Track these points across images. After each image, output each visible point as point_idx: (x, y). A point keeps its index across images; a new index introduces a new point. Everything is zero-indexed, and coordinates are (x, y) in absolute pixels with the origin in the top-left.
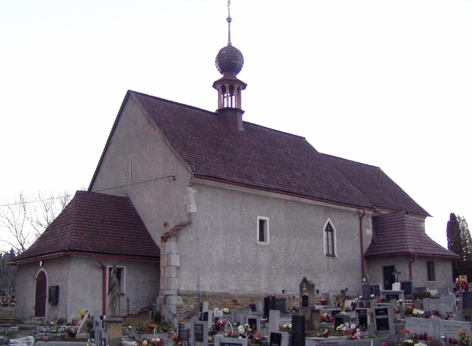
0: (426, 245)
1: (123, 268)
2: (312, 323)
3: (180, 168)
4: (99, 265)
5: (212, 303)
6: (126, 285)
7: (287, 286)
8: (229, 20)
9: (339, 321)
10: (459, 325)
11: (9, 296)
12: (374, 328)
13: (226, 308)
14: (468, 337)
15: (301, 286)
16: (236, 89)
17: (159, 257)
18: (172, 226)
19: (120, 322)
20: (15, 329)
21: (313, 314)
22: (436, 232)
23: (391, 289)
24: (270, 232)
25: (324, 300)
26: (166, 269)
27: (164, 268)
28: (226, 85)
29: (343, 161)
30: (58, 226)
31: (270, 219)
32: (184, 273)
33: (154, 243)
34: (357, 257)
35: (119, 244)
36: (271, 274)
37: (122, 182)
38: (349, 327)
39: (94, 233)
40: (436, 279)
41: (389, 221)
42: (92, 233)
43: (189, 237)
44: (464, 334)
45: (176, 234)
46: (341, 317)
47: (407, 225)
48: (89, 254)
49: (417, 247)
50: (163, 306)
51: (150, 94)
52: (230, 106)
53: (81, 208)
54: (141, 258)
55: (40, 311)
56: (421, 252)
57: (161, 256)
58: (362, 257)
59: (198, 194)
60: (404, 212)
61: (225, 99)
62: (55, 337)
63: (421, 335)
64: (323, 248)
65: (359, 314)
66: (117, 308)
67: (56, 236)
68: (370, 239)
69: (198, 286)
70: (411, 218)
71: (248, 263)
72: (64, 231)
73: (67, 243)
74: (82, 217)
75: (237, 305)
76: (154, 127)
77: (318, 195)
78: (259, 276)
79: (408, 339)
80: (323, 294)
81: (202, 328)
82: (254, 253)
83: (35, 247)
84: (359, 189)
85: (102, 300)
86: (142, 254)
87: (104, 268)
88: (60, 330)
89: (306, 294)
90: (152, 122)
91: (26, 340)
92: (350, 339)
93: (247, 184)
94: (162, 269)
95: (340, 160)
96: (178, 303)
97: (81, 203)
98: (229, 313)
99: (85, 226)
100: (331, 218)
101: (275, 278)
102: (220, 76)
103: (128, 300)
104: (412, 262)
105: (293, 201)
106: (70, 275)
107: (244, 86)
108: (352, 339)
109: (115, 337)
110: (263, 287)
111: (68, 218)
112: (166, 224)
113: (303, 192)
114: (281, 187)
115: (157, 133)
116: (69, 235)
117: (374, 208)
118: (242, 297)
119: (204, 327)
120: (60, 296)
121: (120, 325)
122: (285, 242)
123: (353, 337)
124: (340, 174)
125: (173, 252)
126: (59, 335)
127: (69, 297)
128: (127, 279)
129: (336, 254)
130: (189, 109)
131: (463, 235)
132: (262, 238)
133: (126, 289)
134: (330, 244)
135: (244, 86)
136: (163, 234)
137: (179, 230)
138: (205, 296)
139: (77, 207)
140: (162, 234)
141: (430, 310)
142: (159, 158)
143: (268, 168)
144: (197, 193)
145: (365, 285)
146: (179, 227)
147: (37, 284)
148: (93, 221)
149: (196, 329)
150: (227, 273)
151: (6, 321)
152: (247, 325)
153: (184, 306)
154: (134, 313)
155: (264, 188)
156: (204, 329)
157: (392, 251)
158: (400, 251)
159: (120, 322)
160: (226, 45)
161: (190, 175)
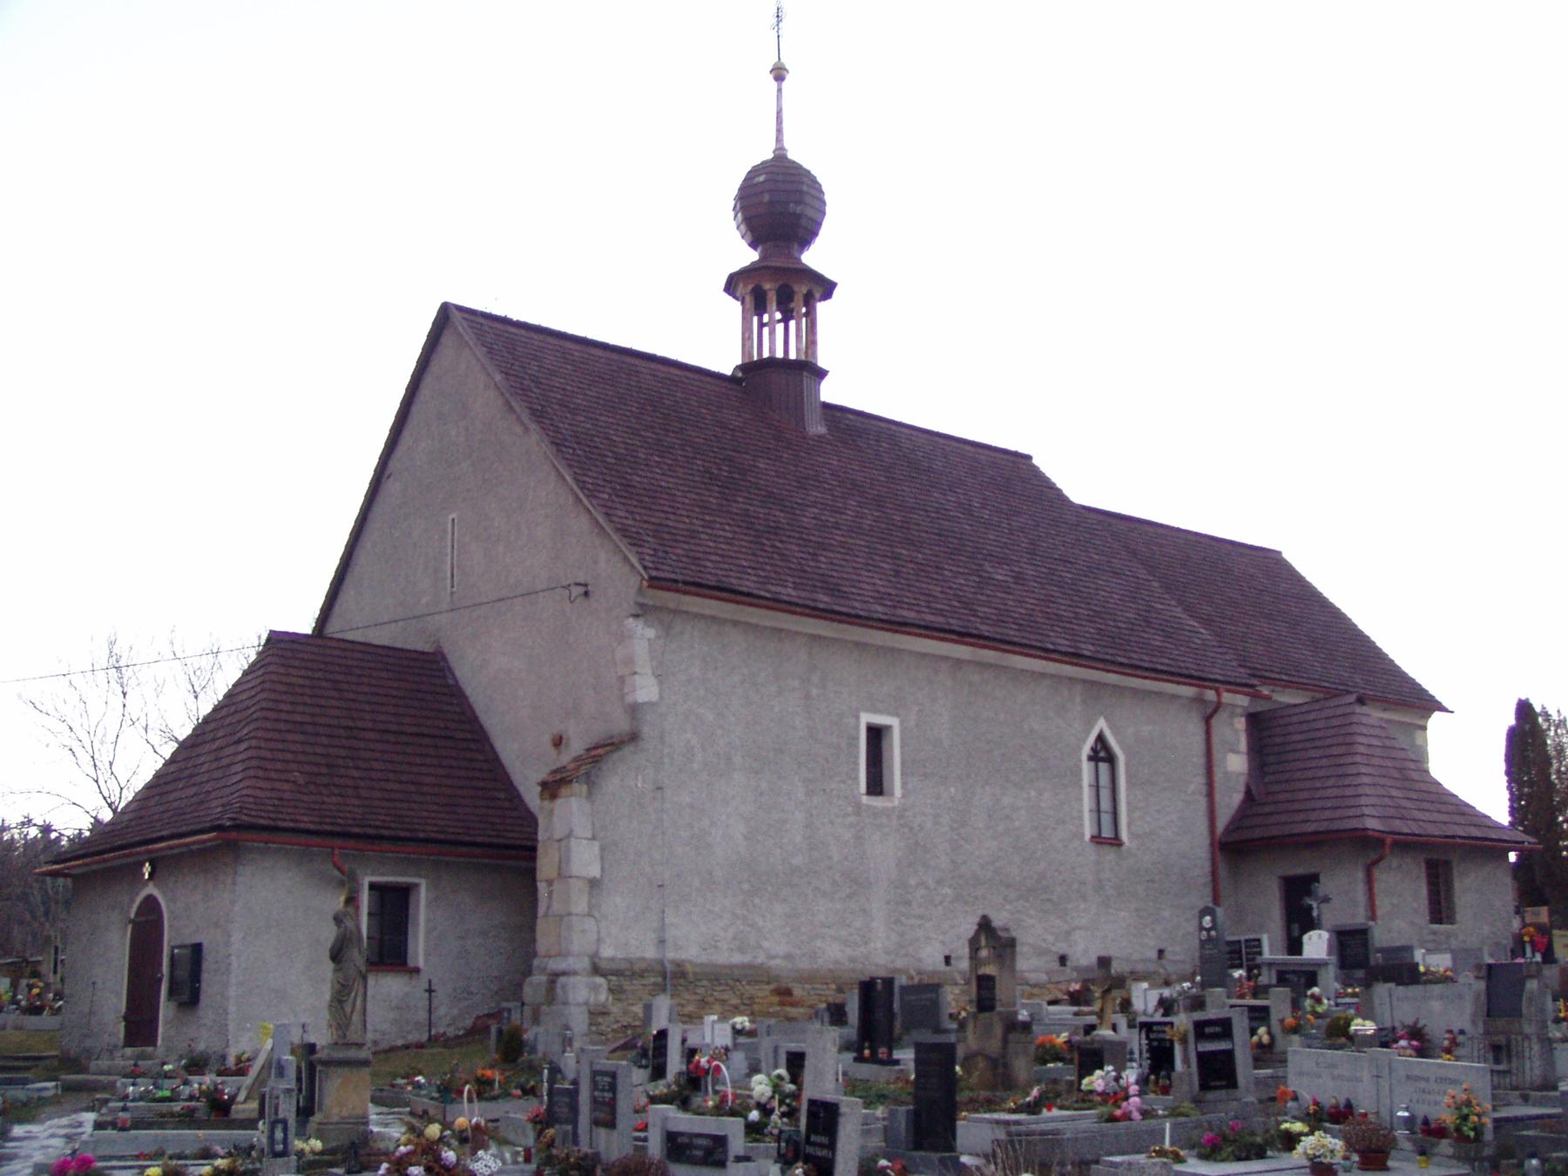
0: (1426, 805)
1: (417, 885)
2: (1006, 1066)
3: (603, 556)
5: (710, 999)
7: (931, 946)
8: (779, 74)
9: (1091, 1058)
10: (1452, 1074)
11: (51, 978)
12: (1191, 1084)
13: (742, 1013)
14: (1479, 1115)
15: (974, 944)
16: (799, 298)
17: (534, 849)
18: (576, 747)
19: (365, 1063)
20: (46, 1089)
21: (1011, 1037)
22: (1468, 766)
23: (1300, 953)
24: (903, 763)
25: (1077, 987)
26: (556, 886)
27: (550, 882)
28: (767, 286)
29: (1160, 531)
30: (207, 747)
31: (902, 723)
32: (617, 902)
34: (1195, 847)
35: (405, 805)
36: (908, 903)
37: (424, 601)
38: (1117, 1079)
39: (324, 770)
40: (1458, 917)
41: (1305, 727)
42: (315, 769)
43: (632, 783)
44: (1468, 1103)
45: (588, 774)
46: (1096, 1045)
47: (1361, 739)
48: (303, 838)
49: (1392, 812)
50: (544, 1008)
51: (515, 316)
52: (780, 354)
53: (283, 688)
54: (478, 850)
55: (140, 1027)
56: (1406, 830)
57: (540, 846)
58: (1212, 844)
59: (661, 642)
60: (1352, 698)
61: (766, 330)
62: (163, 1116)
63: (1336, 1107)
64: (1081, 818)
65: (1148, 1038)
66: (356, 1017)
67: (198, 779)
68: (1242, 789)
69: (662, 942)
70: (1374, 715)
71: (830, 868)
72: (224, 762)
73: (229, 804)
74: (283, 716)
75: (792, 1005)
76: (523, 424)
77: (1063, 644)
78: (864, 911)
79: (1296, 1118)
80: (1076, 969)
81: (613, 1088)
82: (848, 835)
83: (130, 816)
84: (1207, 622)
86: (479, 839)
88: (185, 1091)
89: (989, 970)
90: (517, 409)
91: (70, 1126)
92: (1108, 1121)
93: (824, 610)
94: (542, 887)
95: (1160, 531)
96: (592, 1000)
97: (282, 670)
98: (751, 1033)
99: (294, 747)
100: (1107, 720)
101: (920, 917)
102: (750, 256)
103: (430, 991)
104: (1375, 863)
105: (982, 665)
106: (236, 909)
107: (826, 288)
108: (1112, 1119)
109: (345, 1113)
111: (239, 721)
113: (1012, 633)
114: (941, 619)
115: (534, 443)
116: (239, 777)
117: (1252, 686)
118: (808, 978)
119: (620, 1081)
120: (205, 976)
121: (366, 1070)
122: (953, 799)
123: (1118, 1112)
124: (1142, 573)
125: (578, 831)
126: (177, 1107)
127: (233, 980)
128: (428, 921)
129: (1124, 835)
130: (644, 363)
131: (1558, 771)
132: (876, 785)
133: (427, 954)
134: (1106, 805)
135: (826, 288)
136: (548, 770)
137: (596, 760)
138: (683, 975)
139: (267, 685)
140: (542, 774)
141: (1397, 1024)
142: (538, 527)
143: (896, 557)
144: (658, 637)
145: (1210, 939)
146: (600, 751)
147: (132, 939)
148: (321, 730)
149: (595, 1085)
150: (757, 901)
151: (21, 1064)
152: (782, 1071)
153: (615, 1009)
154: (451, 1032)
155: (882, 621)
156: (619, 1088)
157: (1311, 827)
158: (1336, 826)
159: (365, 1063)
160: (771, 156)
161: (634, 581)
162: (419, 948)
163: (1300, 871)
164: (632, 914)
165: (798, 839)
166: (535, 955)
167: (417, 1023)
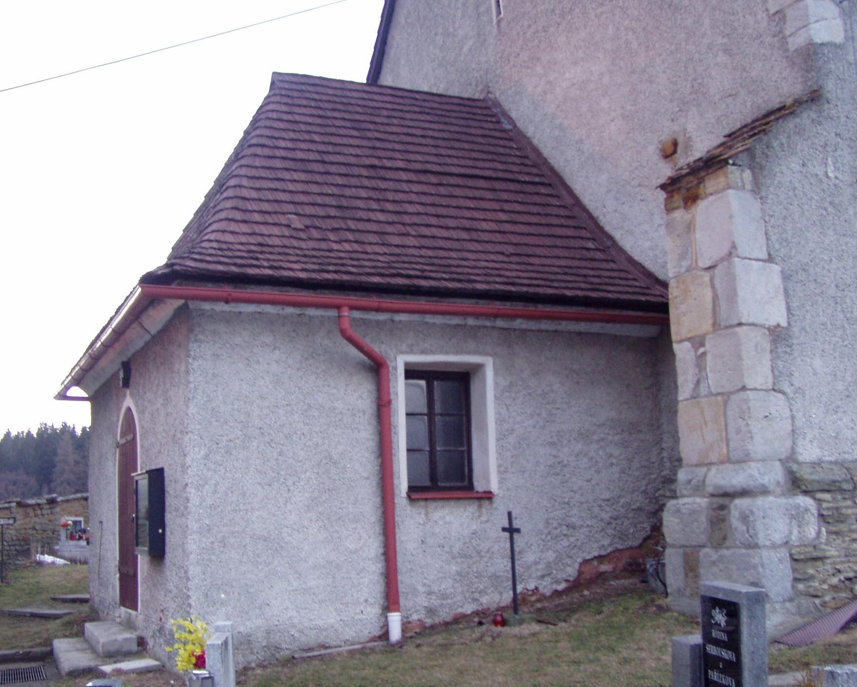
1: (479, 367)
4: (353, 351)
6: (501, 449)
27: (698, 342)
33: (621, 250)
43: (819, 170)
85: (378, 528)
87: (377, 368)
94: (682, 351)
97: (285, 108)
103: (511, 530)
106: (193, 410)
112: (675, 144)
120: (169, 517)
125: (744, 249)
127: (193, 525)
128: (500, 421)
133: (502, 471)
154: (547, 587)
162: (490, 463)
167: (495, 577)
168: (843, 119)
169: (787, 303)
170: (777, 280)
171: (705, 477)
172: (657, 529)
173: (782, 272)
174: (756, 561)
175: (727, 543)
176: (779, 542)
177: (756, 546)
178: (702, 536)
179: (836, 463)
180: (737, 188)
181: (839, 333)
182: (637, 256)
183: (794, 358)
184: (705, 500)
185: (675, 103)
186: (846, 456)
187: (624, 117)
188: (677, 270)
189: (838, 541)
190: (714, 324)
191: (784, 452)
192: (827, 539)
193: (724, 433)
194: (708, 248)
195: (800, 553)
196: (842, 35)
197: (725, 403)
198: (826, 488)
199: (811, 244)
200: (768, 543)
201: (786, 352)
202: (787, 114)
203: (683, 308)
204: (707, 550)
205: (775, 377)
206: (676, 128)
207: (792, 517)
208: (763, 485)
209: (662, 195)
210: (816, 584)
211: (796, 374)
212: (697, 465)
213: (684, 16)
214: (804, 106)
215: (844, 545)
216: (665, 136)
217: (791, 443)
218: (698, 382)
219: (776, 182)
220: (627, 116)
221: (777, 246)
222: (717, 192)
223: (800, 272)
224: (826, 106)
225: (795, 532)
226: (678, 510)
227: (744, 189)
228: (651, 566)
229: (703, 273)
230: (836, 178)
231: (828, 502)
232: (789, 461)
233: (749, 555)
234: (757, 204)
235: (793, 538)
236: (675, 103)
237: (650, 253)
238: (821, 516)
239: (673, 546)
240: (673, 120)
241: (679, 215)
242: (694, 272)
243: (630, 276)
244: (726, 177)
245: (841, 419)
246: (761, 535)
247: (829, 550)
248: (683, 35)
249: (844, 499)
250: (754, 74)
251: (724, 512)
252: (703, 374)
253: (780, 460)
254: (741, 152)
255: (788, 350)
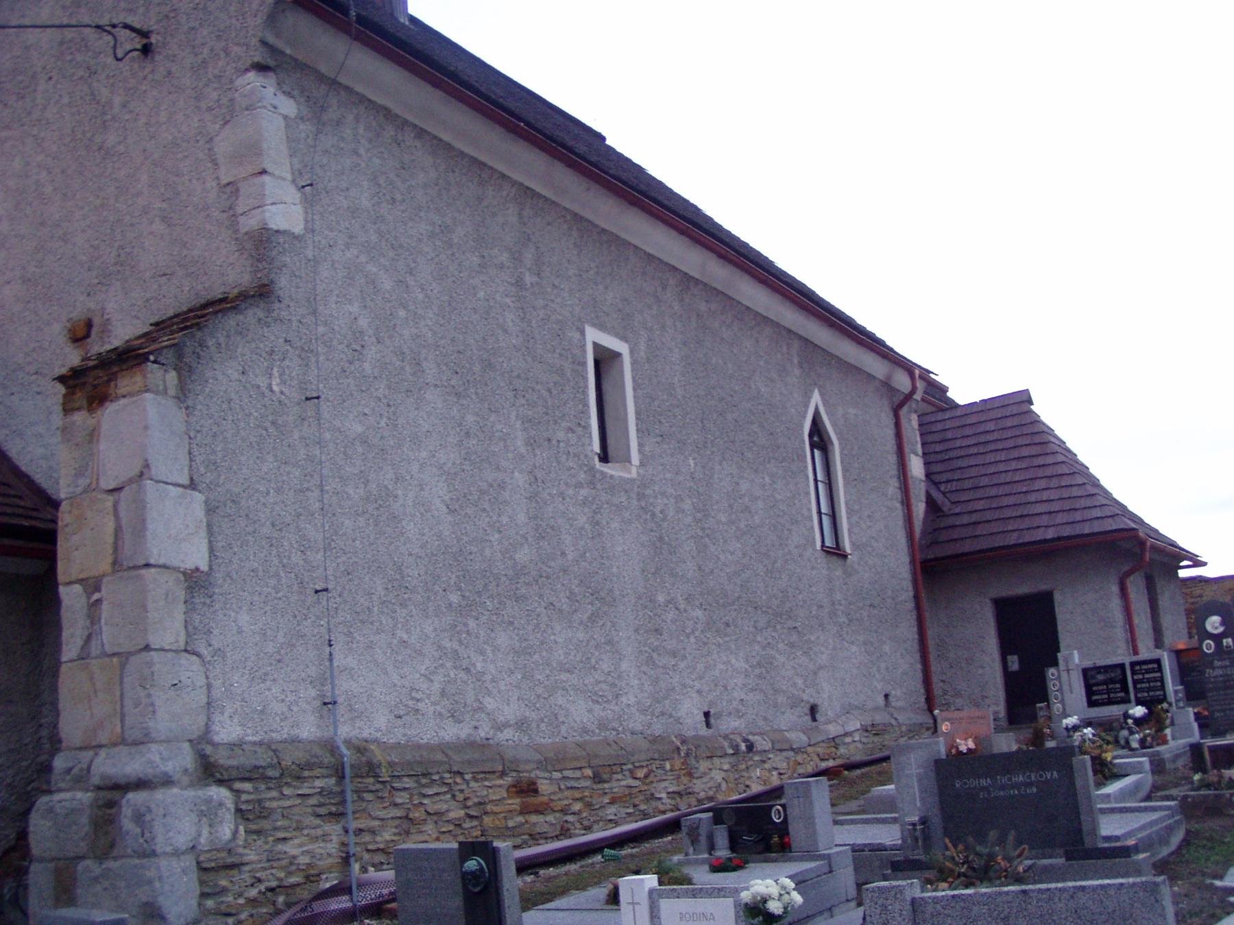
5: (417, 814)
24: (638, 413)
27: (92, 585)
32: (240, 623)
43: (262, 382)
45: (177, 348)
69: (329, 704)
75: (538, 812)
94: (71, 597)
110: (632, 700)
112: (89, 325)
118: (554, 761)
125: (160, 469)
138: (372, 769)
150: (472, 624)
163: (1023, 589)
164: (270, 648)
165: (521, 518)
166: (56, 743)
168: (295, 324)
169: (210, 542)
170: (199, 512)
171: (92, 761)
172: (23, 835)
173: (206, 502)
174: (151, 874)
175: (115, 853)
176: (184, 848)
177: (154, 854)
178: (82, 844)
179: (261, 743)
180: (157, 393)
181: (272, 582)
182: (24, 465)
183: (216, 611)
184: (89, 794)
185: (94, 273)
186: (274, 735)
187: (25, 280)
188: (71, 490)
189: (259, 843)
190: (114, 563)
191: (195, 730)
192: (246, 840)
193: (118, 707)
194: (114, 464)
195: (210, 860)
196: (302, 226)
197: (123, 666)
198: (247, 775)
199: (245, 471)
200: (169, 849)
201: (204, 604)
202: (229, 309)
203: (75, 539)
204: (88, 862)
205: (188, 635)
206: (92, 305)
207: (202, 814)
208: (166, 774)
209: (61, 389)
210: (230, 899)
211: (216, 632)
212: (80, 749)
213: (116, 165)
214: (250, 301)
215: (267, 847)
216: (78, 314)
217: (205, 719)
218: (89, 638)
219: (207, 390)
220: (29, 280)
221: (202, 470)
222: (131, 395)
223: (229, 504)
224: (277, 305)
225: (205, 832)
226: (51, 810)
227: (166, 393)
228: (10, 889)
229: (105, 496)
230: (282, 393)
231: (249, 793)
232: (202, 743)
233: (142, 867)
234: (181, 415)
235: (202, 840)
236: (94, 273)
237: (43, 463)
238: (238, 811)
239: (41, 860)
240: (89, 295)
241: (79, 417)
242: (94, 494)
243: (13, 493)
244: (144, 376)
245: (269, 689)
246: (160, 839)
247: (247, 855)
248: (113, 189)
249: (269, 789)
250: (195, 252)
251: (114, 810)
252: (96, 627)
253: (190, 741)
254: (166, 347)
255: (208, 601)
